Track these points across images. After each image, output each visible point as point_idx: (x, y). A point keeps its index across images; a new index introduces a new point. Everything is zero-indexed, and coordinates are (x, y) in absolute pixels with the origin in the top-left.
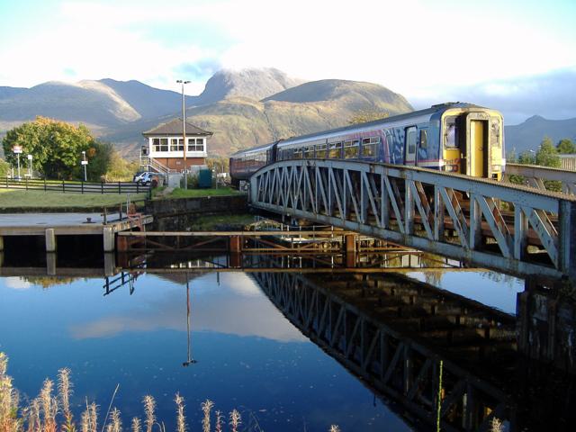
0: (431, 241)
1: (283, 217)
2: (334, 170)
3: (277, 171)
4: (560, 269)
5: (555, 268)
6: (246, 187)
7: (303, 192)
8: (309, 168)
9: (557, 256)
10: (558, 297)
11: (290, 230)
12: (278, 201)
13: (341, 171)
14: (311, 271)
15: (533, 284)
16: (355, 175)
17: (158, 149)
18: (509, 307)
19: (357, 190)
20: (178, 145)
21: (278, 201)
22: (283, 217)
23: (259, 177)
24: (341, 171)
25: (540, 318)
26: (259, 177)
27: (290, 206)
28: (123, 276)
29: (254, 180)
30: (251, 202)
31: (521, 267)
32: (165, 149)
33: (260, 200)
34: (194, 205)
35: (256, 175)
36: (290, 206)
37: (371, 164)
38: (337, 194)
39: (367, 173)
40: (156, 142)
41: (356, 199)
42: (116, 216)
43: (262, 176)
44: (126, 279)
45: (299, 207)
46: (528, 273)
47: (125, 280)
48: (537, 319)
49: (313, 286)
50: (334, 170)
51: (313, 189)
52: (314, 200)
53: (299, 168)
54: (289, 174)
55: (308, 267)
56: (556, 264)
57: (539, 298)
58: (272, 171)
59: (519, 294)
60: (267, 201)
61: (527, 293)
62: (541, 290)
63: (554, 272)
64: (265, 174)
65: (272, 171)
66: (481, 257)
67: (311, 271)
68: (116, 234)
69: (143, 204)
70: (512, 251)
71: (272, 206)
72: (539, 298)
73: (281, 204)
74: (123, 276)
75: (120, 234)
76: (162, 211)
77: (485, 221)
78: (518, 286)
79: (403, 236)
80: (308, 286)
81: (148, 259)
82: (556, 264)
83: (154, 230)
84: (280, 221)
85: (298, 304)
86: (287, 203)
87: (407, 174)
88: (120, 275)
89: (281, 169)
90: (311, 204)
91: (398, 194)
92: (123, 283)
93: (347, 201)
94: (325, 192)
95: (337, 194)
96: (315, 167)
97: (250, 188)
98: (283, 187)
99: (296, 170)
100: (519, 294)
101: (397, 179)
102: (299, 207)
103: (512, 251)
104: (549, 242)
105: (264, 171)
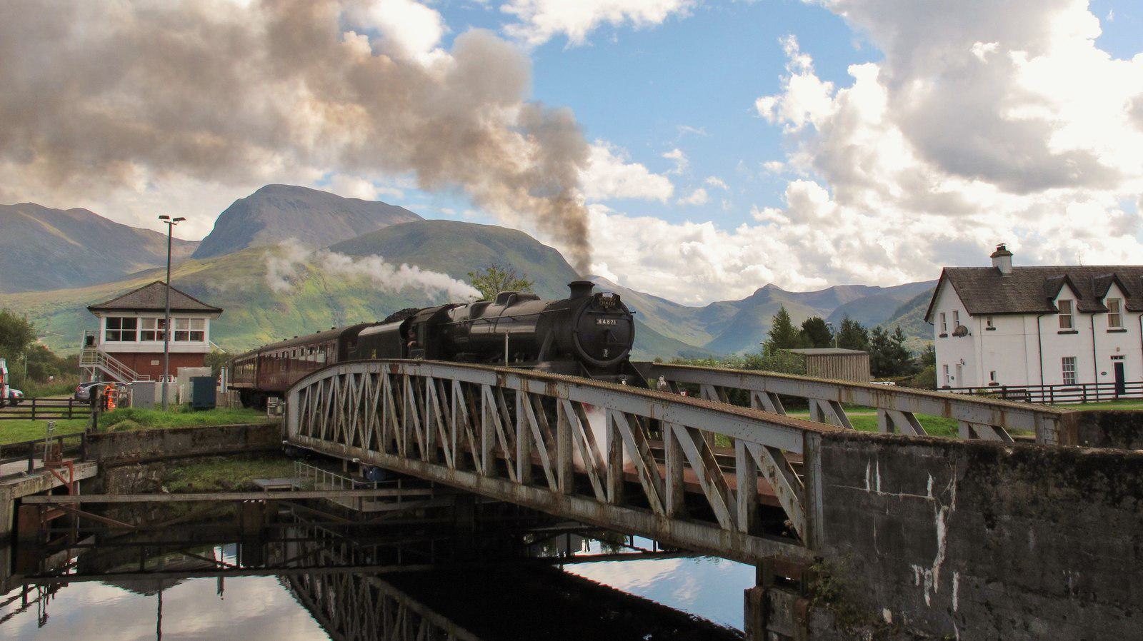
0: (601, 504)
1: (345, 465)
2: (436, 380)
3: (336, 382)
4: (810, 547)
5: (803, 545)
6: (279, 410)
7: (381, 418)
8: (391, 376)
9: (805, 525)
10: (913, 320)
11: (357, 488)
12: (336, 435)
13: (448, 384)
14: (394, 568)
15: (770, 576)
16: (472, 390)
17: (116, 337)
18: (731, 616)
19: (474, 421)
20: (156, 329)
21: (336, 435)
22: (345, 465)
23: (303, 392)
24: (448, 384)
25: (784, 632)
26: (303, 392)
27: (357, 443)
28: (24, 595)
29: (293, 398)
30: (286, 437)
31: (749, 545)
32: (130, 337)
33: (304, 432)
34: (182, 442)
35: (299, 388)
36: (357, 443)
37: (498, 372)
38: (440, 426)
39: (493, 388)
40: (112, 323)
41: (474, 434)
42: (22, 465)
43: (309, 390)
44: (32, 596)
45: (374, 447)
46: (761, 555)
47: (29, 600)
48: (779, 635)
49: (397, 596)
50: (436, 380)
51: (399, 415)
52: (401, 431)
53: (374, 376)
54: (358, 387)
55: (397, 485)
56: (804, 538)
57: (781, 598)
58: (327, 381)
59: (748, 593)
60: (316, 435)
61: (760, 591)
62: (781, 583)
63: (802, 552)
64: (315, 385)
65: (327, 381)
66: (691, 532)
67: (394, 568)
68: (18, 502)
69: (78, 441)
70: (734, 521)
71: (326, 444)
72: (781, 598)
73: (341, 440)
74: (24, 595)
75: (24, 500)
76: (110, 403)
77: (689, 466)
78: (746, 576)
79: (555, 497)
80: (388, 597)
81: (78, 565)
82: (804, 538)
83: (98, 491)
84: (339, 471)
85: (369, 631)
86: (352, 439)
87: (560, 390)
88: (20, 590)
89: (342, 378)
90: (394, 442)
91: (544, 417)
92: (25, 605)
93: (458, 436)
94: (420, 417)
95: (440, 426)
96: (403, 375)
97: (286, 409)
98: (346, 409)
99: (369, 381)
100: (748, 593)
101: (544, 398)
102: (374, 447)
103: (734, 521)
104: (792, 501)
105: (314, 380)
